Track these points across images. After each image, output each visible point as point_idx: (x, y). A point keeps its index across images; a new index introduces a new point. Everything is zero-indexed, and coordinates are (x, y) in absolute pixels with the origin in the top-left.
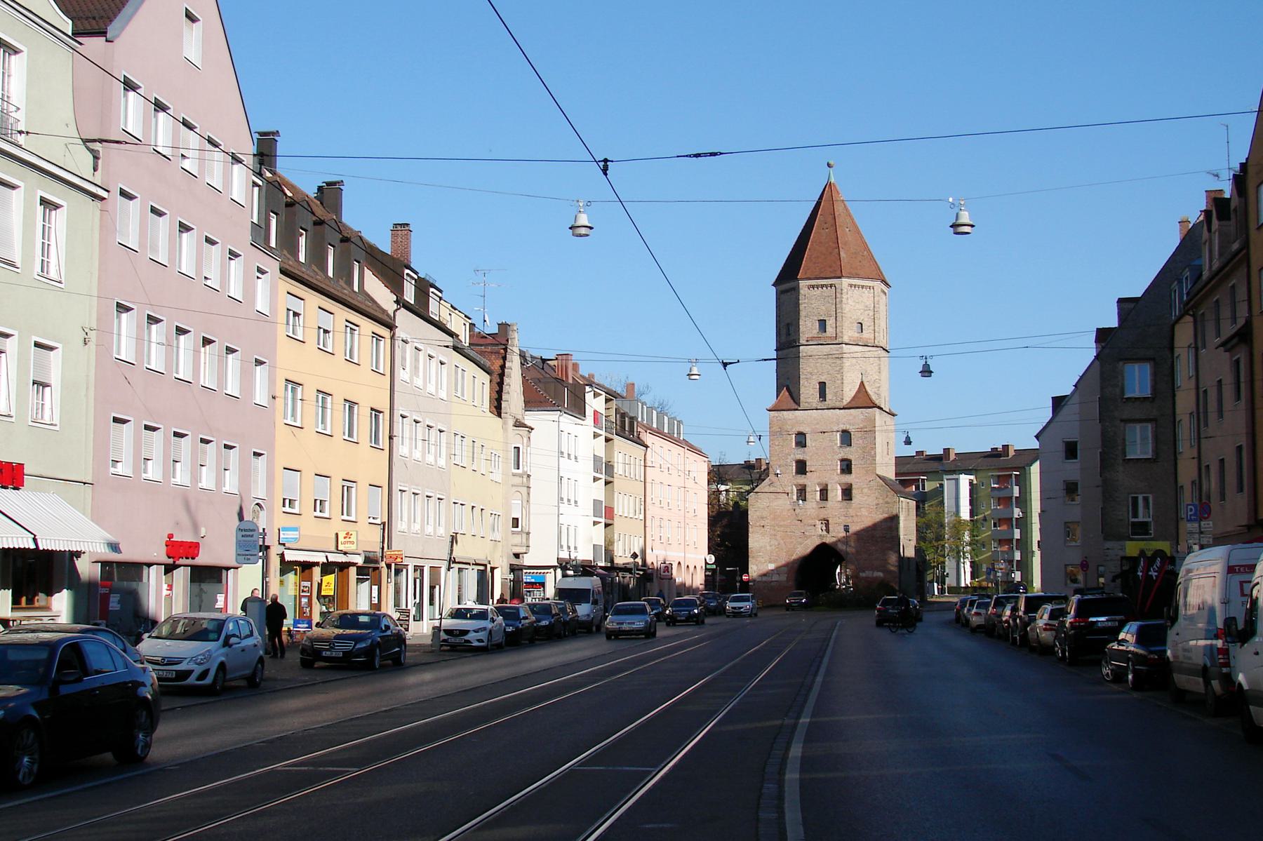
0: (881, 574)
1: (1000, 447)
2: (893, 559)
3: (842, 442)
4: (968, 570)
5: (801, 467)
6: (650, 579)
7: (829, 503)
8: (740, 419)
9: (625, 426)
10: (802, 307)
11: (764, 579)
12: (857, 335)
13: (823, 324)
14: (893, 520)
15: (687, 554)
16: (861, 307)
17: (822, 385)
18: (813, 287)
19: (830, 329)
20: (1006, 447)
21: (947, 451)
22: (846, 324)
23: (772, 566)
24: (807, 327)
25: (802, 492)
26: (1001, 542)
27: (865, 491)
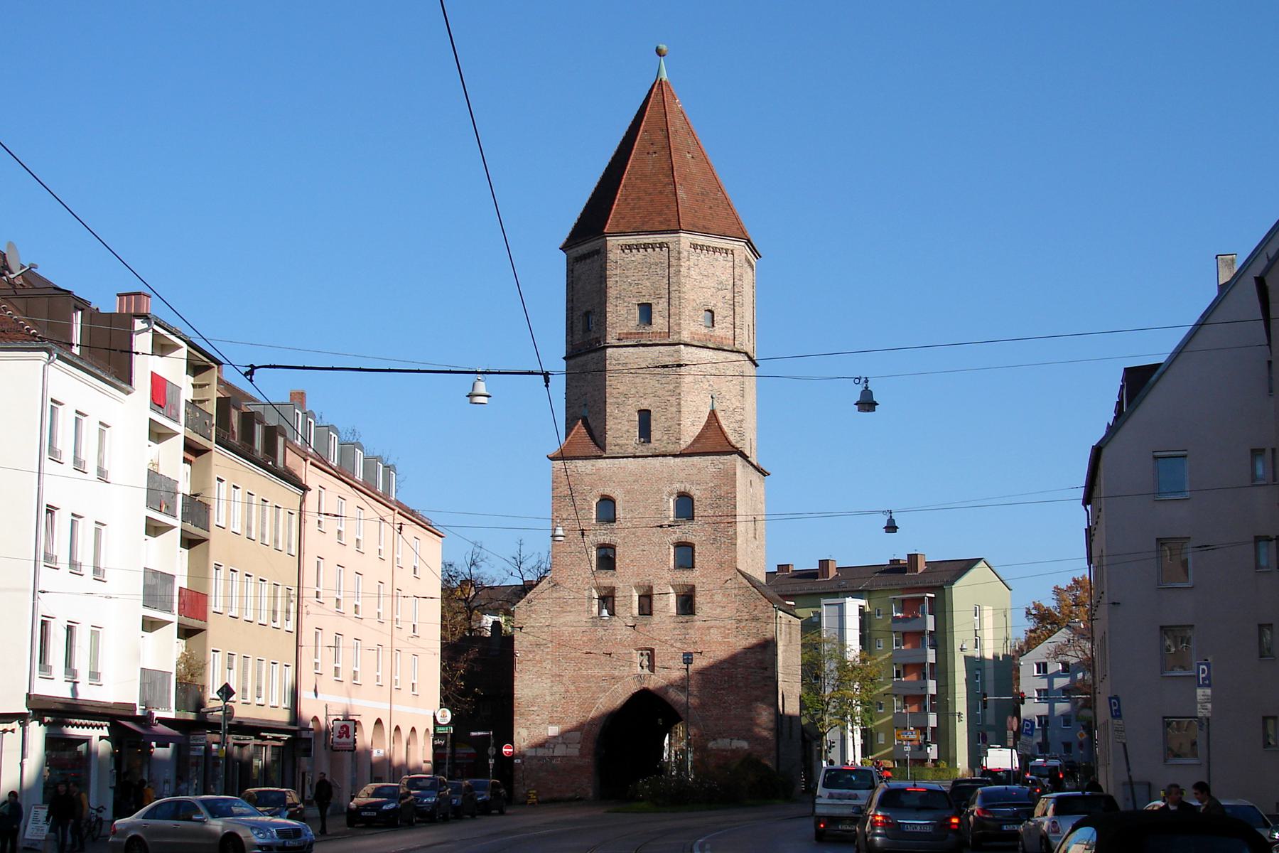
0: (744, 745)
1: (904, 558)
2: (764, 716)
3: (678, 514)
4: (859, 741)
5: (607, 559)
6: (309, 756)
7: (656, 618)
8: (512, 514)
9: (245, 430)
10: (610, 282)
11: (541, 752)
12: (704, 330)
13: (646, 311)
14: (767, 647)
15: (397, 705)
16: (711, 283)
17: (645, 416)
18: (630, 247)
19: (659, 322)
20: (913, 558)
21: (824, 564)
22: (687, 311)
23: (553, 731)
24: (620, 316)
25: (607, 598)
26: (907, 699)
27: (718, 598)
